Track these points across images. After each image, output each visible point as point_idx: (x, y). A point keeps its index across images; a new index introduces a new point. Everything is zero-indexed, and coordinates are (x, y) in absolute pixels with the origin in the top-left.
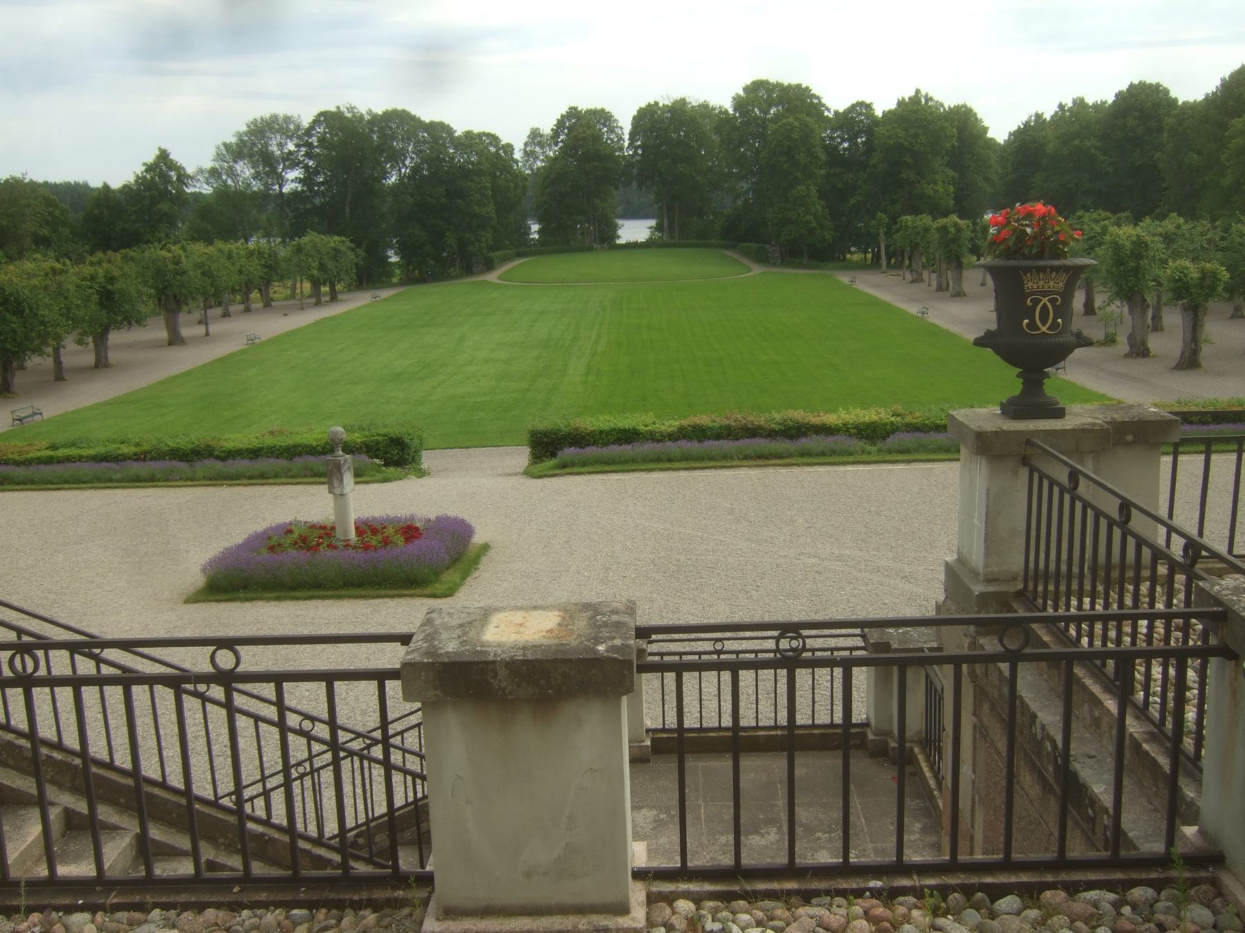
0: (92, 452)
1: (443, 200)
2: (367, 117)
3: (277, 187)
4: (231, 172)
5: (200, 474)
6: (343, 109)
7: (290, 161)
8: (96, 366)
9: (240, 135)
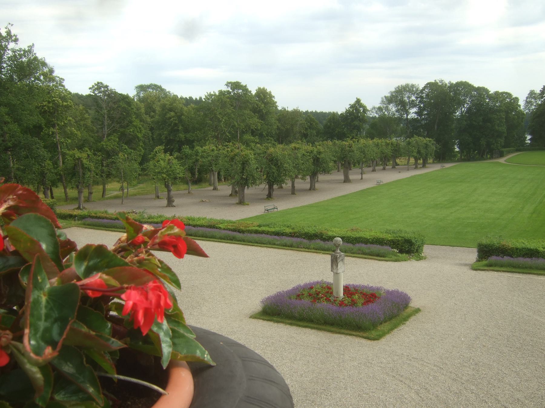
0: (273, 230)
1: (481, 123)
2: (448, 85)
3: (405, 115)
4: (387, 109)
5: (312, 246)
6: (437, 81)
7: (413, 104)
8: (310, 189)
9: (391, 93)
